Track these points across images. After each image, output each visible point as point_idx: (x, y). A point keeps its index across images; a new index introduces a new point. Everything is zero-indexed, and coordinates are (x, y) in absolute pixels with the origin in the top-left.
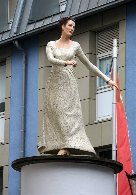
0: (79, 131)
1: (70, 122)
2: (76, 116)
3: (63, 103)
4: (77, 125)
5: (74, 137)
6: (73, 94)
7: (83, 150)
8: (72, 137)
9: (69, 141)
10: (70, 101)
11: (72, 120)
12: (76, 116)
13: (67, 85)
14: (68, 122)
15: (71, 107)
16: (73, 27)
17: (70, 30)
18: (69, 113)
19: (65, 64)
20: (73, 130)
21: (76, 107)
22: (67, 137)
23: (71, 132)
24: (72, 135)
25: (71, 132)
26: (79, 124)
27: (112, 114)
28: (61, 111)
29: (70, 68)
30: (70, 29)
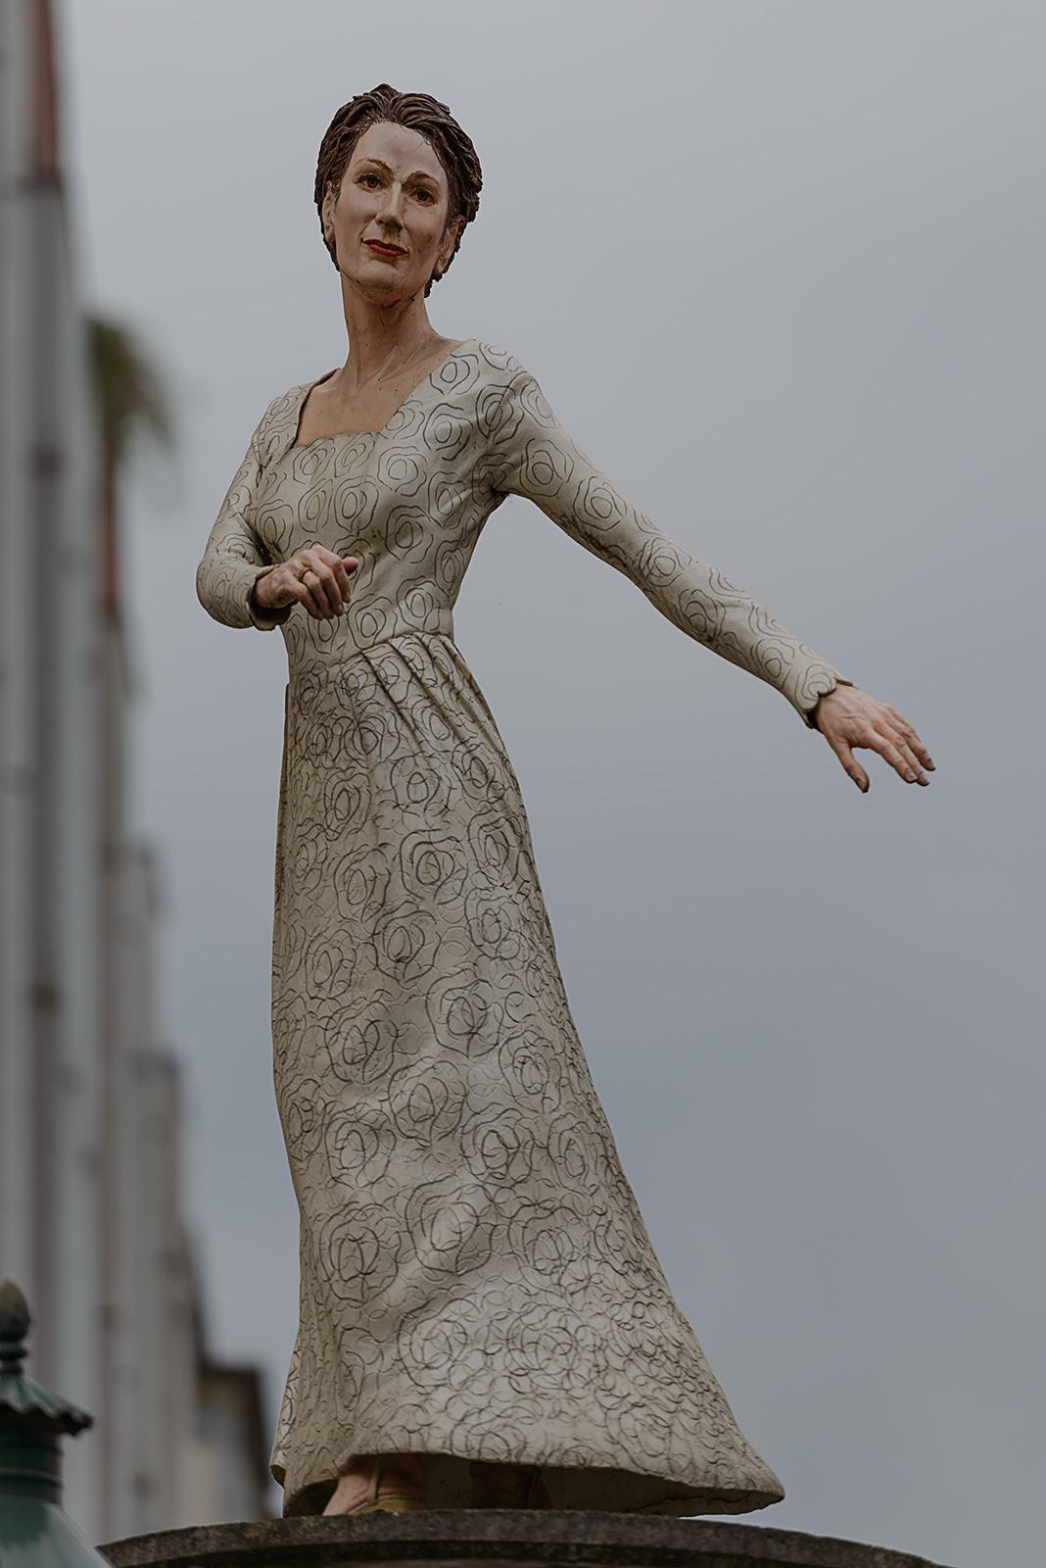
0: (488, 1270)
1: (380, 1194)
2: (443, 1123)
3: (326, 1009)
4: (462, 1215)
5: (426, 1340)
6: (398, 893)
7: (488, 1456)
8: (405, 1340)
9: (377, 1382)
10: (378, 980)
11: (404, 1167)
12: (443, 1123)
13: (350, 816)
14: (364, 1199)
15: (387, 1039)
16: (397, 187)
17: (374, 231)
18: (372, 1106)
19: (253, 596)
20: (411, 1270)
21: (442, 1029)
22: (367, 1351)
23: (397, 1293)
24: (404, 1321)
25: (397, 1293)
26: (478, 1201)
27: (390, 692)
28: (307, 1091)
29: (386, 633)
30: (371, 217)
